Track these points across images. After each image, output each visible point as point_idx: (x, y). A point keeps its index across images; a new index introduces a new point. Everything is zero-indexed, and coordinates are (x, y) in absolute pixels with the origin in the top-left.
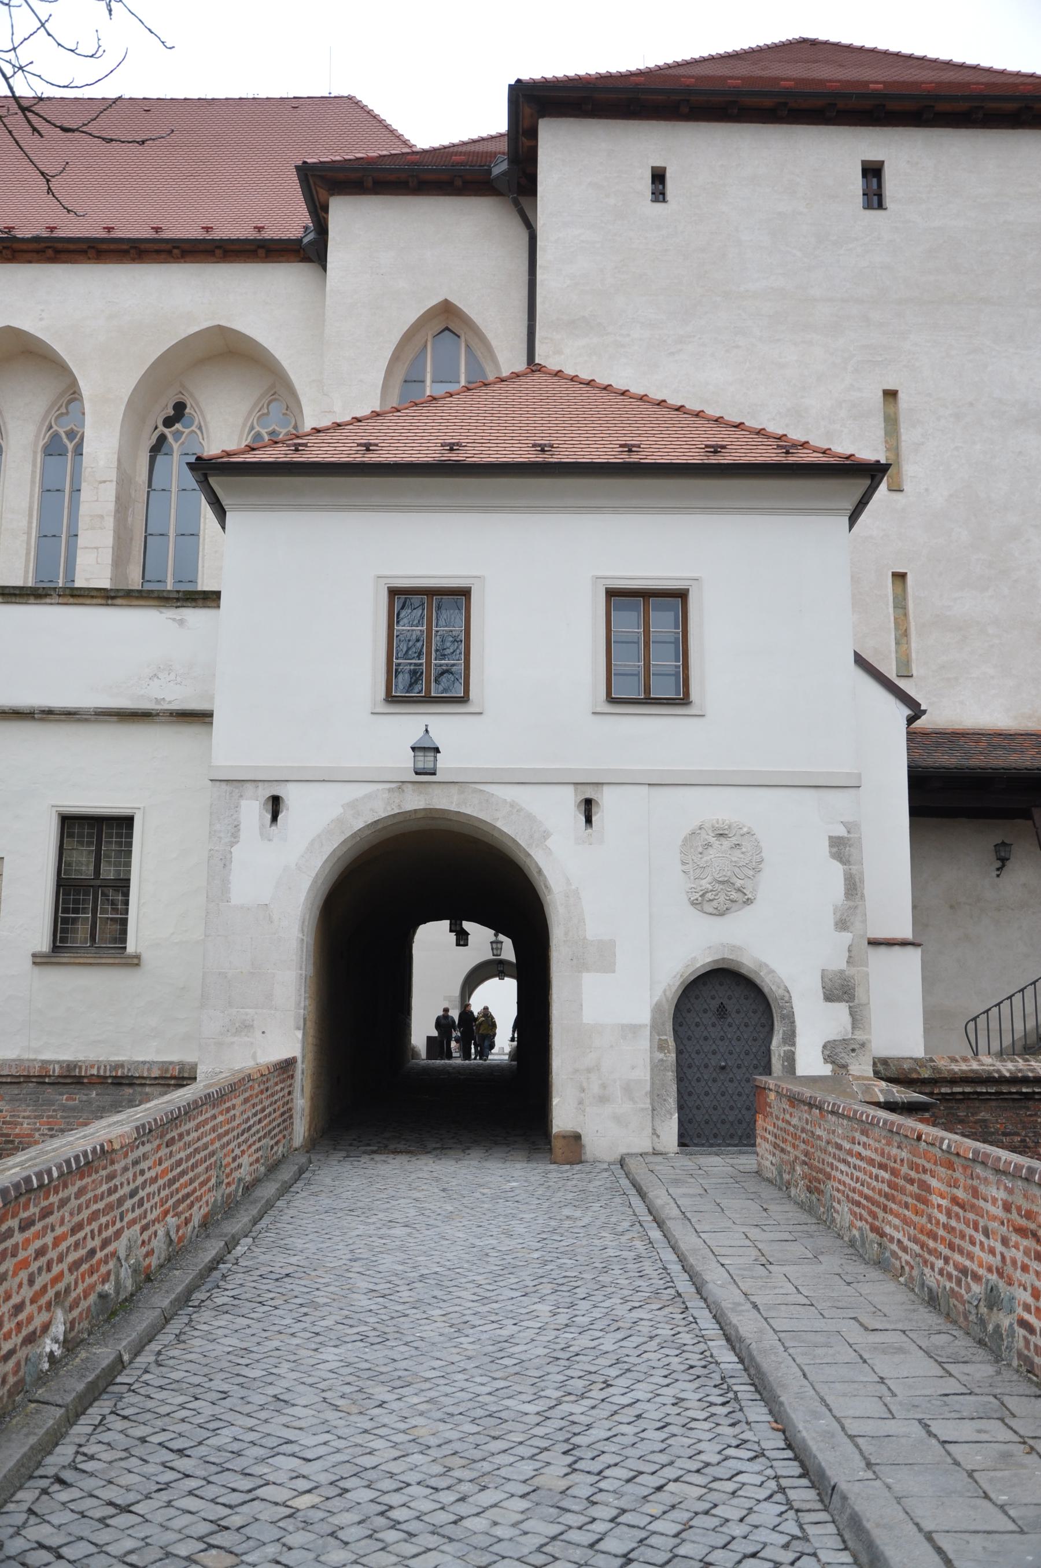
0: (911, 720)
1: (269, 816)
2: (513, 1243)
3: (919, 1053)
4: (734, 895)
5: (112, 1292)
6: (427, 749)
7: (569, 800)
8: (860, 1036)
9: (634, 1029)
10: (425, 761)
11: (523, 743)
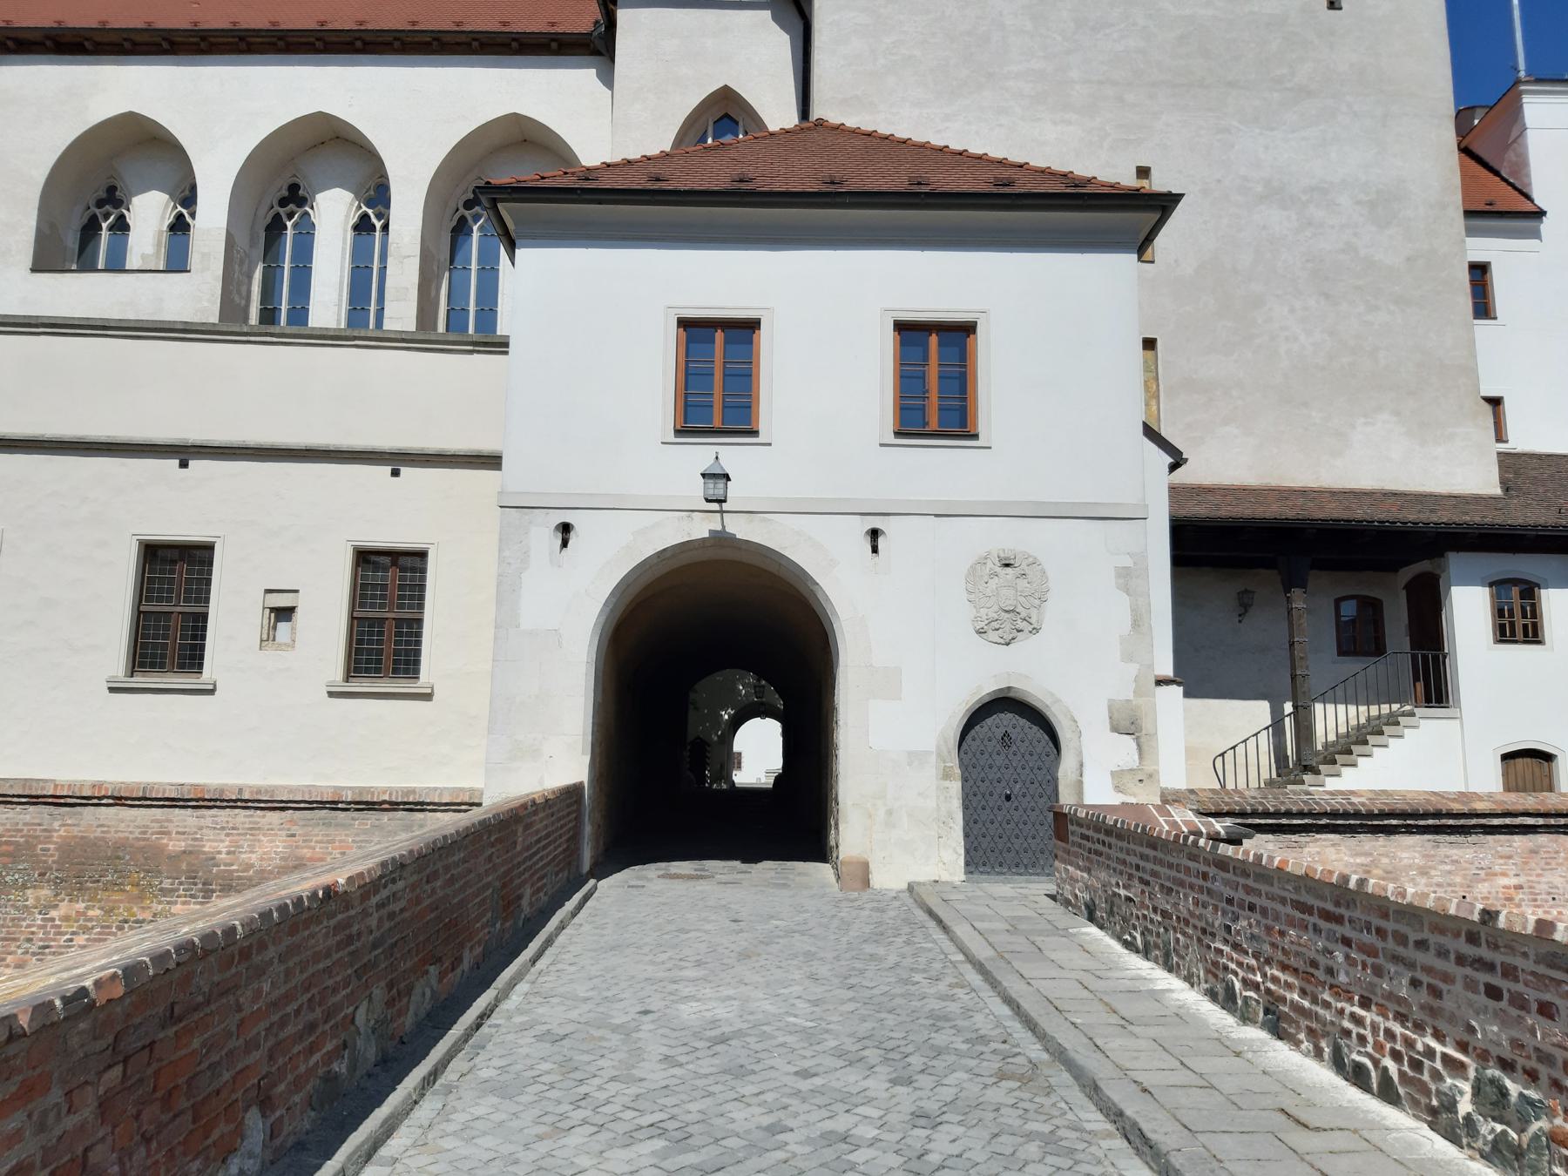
0: (1173, 467)
4: (1021, 625)
5: (344, 1070)
8: (1149, 768)
10: (717, 489)
11: (813, 479)
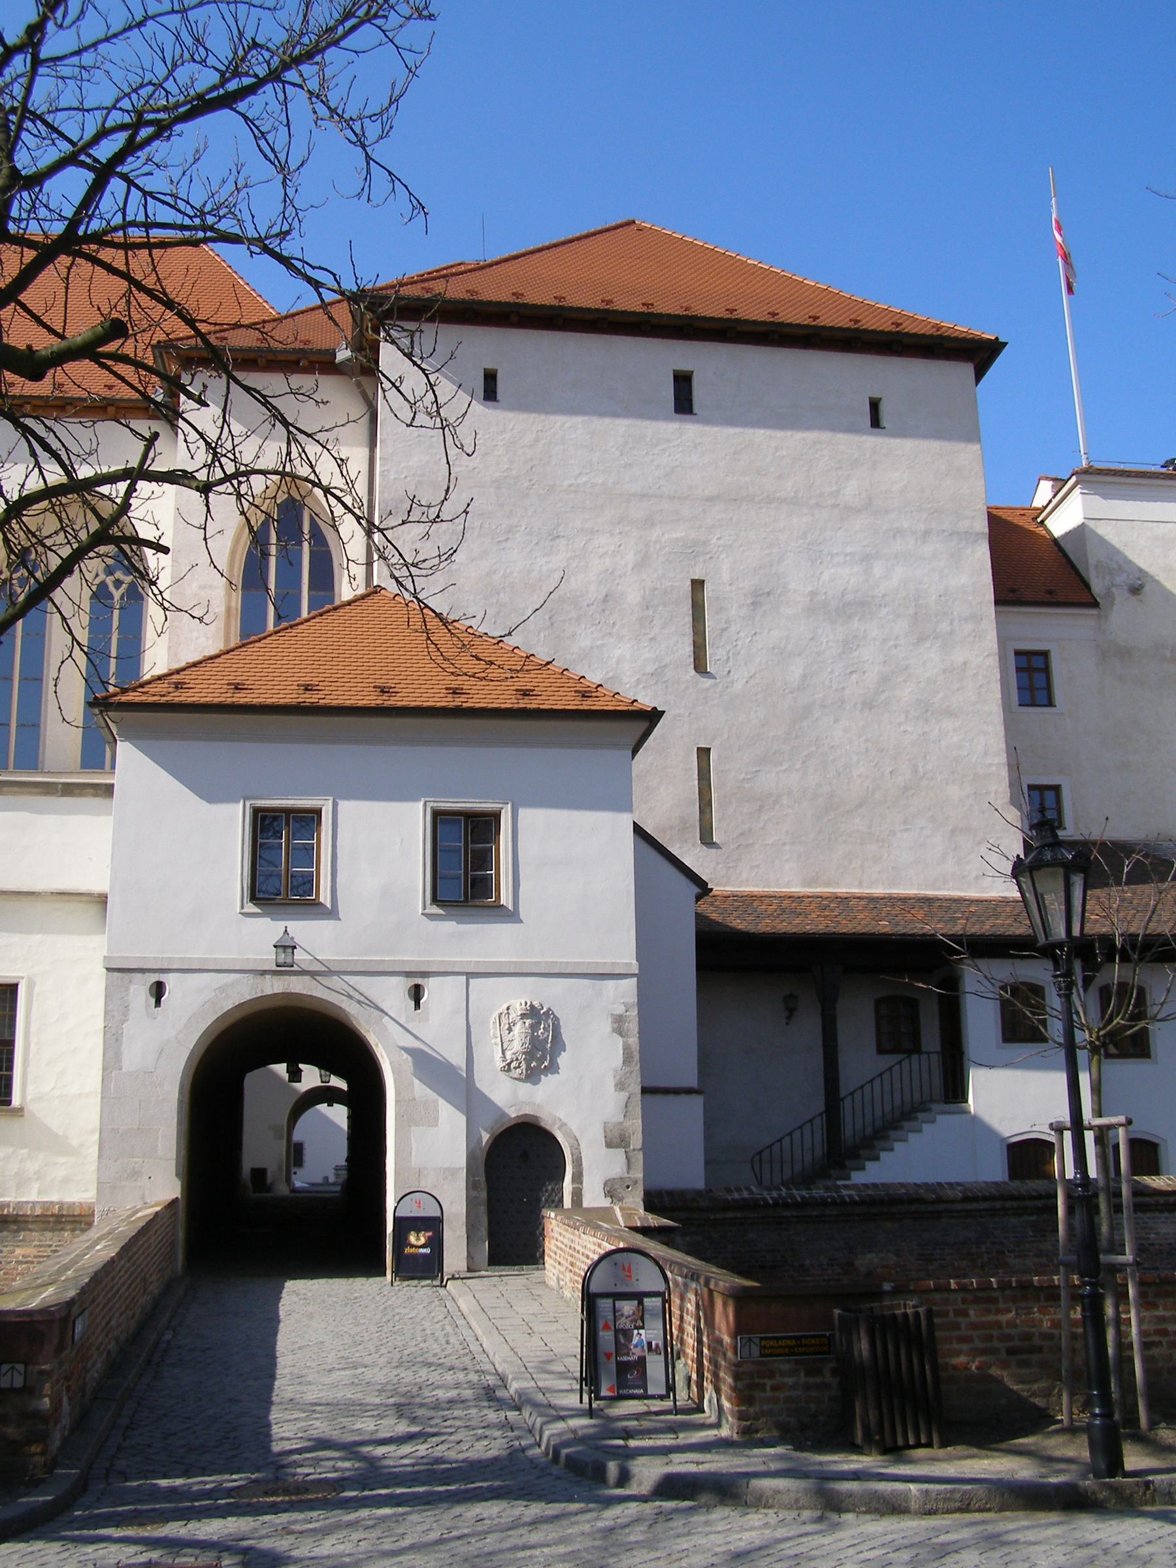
0: (698, 898)
1: (153, 1001)
2: (358, 1329)
3: (700, 1184)
6: (286, 946)
7: (405, 984)
9: (453, 1171)
